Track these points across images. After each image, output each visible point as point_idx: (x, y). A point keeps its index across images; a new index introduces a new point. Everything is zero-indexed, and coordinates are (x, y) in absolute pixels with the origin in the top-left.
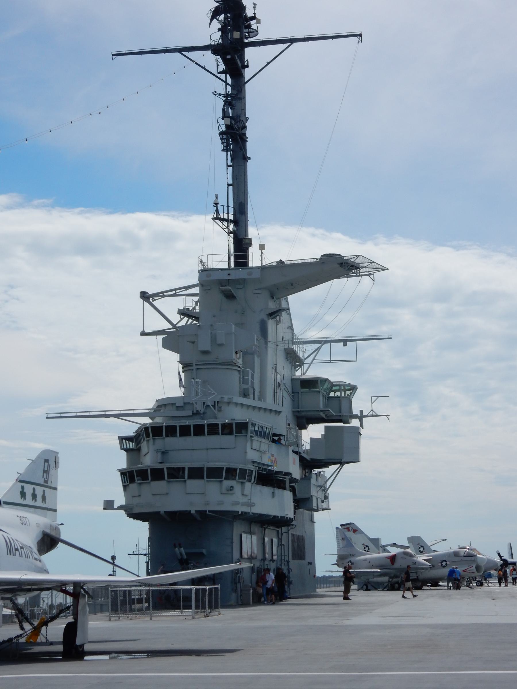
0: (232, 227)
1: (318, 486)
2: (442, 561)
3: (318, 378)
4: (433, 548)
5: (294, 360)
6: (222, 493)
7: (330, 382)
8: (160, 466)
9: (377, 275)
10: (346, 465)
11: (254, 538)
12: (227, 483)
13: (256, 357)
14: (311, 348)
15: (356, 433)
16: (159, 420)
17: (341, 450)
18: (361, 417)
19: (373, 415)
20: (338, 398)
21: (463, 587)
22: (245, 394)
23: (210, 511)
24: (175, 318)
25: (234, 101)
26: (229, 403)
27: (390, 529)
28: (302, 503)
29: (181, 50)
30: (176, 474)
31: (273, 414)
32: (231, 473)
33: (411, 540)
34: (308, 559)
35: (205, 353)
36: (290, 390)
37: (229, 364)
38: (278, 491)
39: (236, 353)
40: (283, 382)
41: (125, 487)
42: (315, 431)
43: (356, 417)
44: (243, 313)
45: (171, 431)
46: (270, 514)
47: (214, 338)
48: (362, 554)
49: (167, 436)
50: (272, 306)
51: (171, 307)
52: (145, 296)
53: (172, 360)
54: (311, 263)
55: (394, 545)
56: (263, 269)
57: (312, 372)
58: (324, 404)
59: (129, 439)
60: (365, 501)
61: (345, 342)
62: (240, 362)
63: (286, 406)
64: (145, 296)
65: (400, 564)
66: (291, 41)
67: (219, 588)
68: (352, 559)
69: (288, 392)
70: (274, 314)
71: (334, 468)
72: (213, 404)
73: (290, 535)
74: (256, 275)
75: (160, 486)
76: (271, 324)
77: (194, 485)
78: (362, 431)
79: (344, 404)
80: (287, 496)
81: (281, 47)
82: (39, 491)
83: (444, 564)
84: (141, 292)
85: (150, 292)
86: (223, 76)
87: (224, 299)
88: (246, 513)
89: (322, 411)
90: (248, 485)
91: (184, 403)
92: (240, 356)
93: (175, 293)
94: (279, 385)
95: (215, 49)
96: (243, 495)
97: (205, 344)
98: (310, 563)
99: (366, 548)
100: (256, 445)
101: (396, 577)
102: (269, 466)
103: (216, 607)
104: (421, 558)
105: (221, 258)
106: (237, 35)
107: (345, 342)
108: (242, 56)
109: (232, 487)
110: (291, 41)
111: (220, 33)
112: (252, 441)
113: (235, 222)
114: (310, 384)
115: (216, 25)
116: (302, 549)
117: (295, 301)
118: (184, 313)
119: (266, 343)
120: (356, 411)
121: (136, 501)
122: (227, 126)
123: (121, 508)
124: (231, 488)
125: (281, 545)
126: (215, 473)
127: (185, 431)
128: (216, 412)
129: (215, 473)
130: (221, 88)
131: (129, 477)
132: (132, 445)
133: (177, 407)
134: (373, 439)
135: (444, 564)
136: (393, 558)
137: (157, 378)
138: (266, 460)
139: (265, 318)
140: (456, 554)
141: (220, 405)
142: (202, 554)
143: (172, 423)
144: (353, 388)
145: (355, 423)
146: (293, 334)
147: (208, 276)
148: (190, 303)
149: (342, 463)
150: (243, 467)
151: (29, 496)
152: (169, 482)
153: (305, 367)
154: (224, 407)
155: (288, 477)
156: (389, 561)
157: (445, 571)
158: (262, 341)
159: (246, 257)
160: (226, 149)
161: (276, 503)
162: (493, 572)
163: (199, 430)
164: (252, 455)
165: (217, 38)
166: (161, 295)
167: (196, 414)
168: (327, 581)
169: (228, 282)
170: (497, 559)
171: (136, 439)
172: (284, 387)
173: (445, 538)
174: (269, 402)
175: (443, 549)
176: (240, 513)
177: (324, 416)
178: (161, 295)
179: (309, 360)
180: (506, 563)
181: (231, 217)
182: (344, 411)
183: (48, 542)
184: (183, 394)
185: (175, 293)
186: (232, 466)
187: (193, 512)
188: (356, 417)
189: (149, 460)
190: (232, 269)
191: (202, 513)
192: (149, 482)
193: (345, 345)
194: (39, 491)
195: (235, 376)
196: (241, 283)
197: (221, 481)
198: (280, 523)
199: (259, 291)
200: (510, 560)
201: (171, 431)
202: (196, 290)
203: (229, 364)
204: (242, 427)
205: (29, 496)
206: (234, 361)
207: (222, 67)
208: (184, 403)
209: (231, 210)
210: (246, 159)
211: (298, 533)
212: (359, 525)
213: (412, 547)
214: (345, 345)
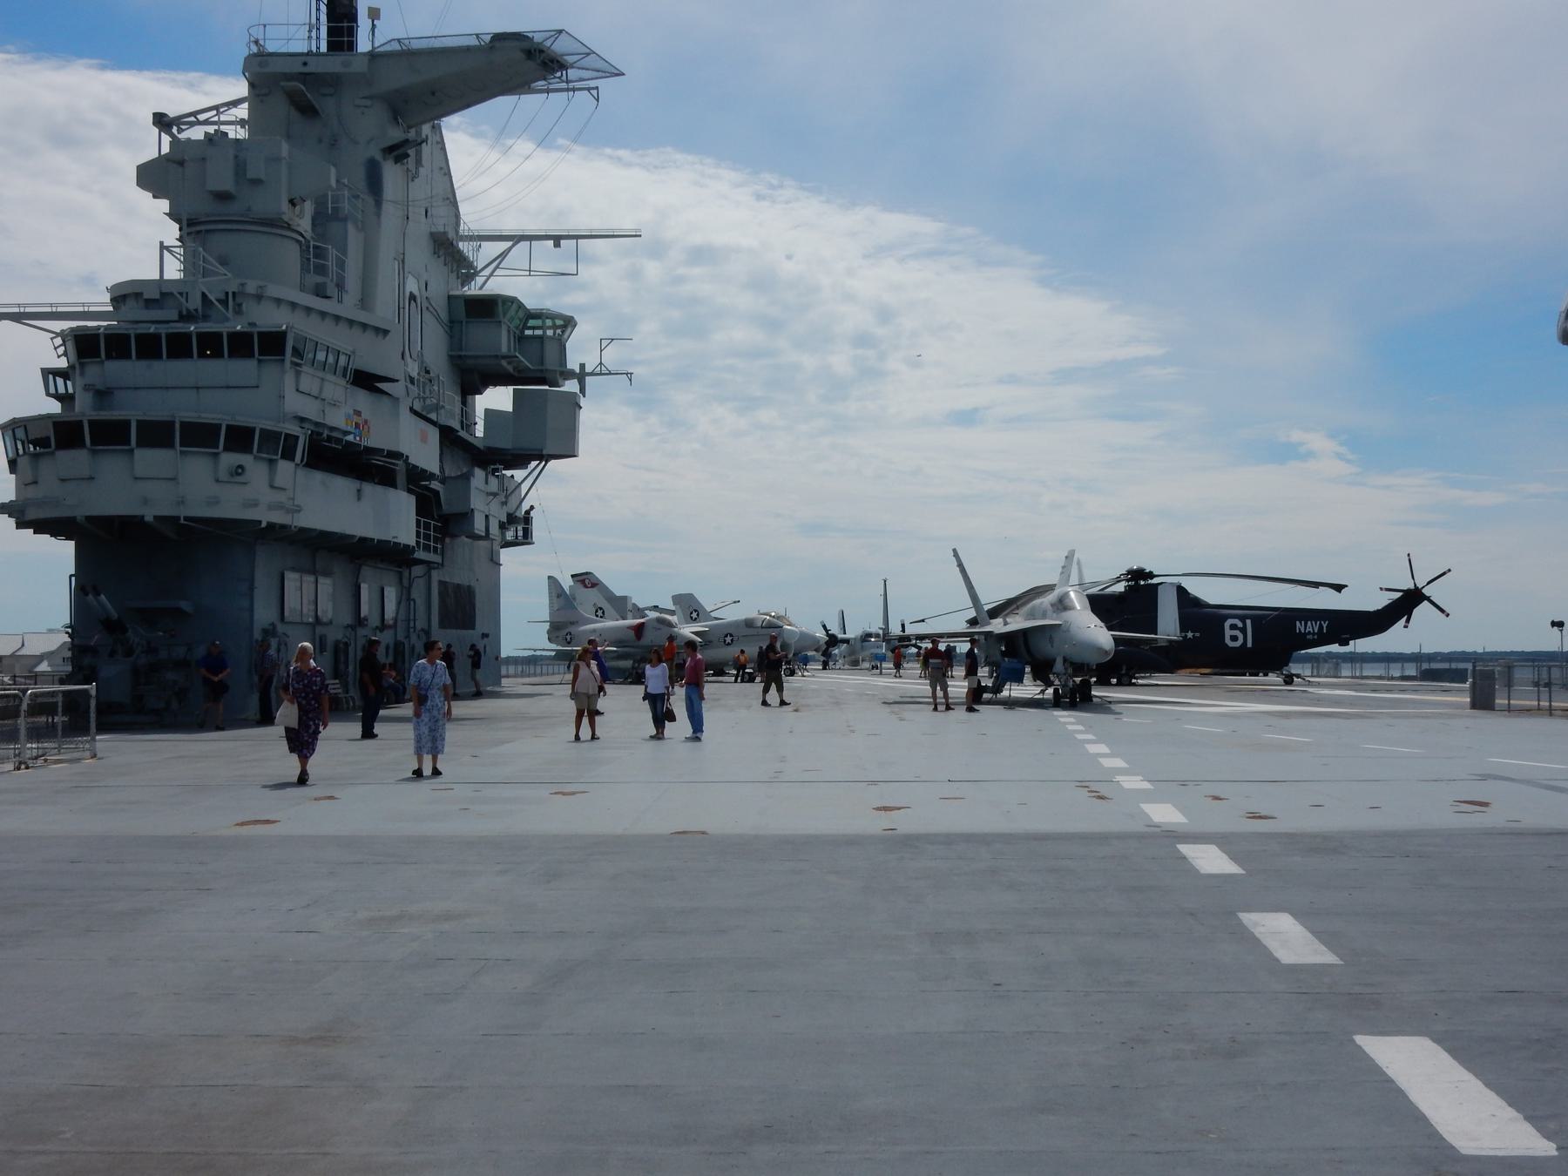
1: (489, 494)
2: (729, 634)
3: (499, 296)
5: (463, 268)
6: (217, 481)
7: (521, 306)
10: (552, 463)
11: (325, 585)
12: (229, 459)
13: (351, 228)
14: (492, 249)
17: (543, 436)
18: (581, 376)
20: (541, 338)
23: (186, 519)
26: (259, 297)
27: (646, 581)
28: (443, 520)
31: (370, 334)
32: (240, 438)
33: (677, 599)
34: (481, 626)
35: (223, 197)
36: (444, 315)
37: (275, 224)
38: (368, 488)
39: (292, 202)
40: (425, 294)
42: (498, 398)
43: (570, 375)
44: (334, 143)
46: (348, 532)
49: (109, 357)
50: (395, 134)
54: (468, 49)
55: (656, 608)
57: (498, 285)
58: (513, 357)
61: (558, 240)
62: (305, 225)
63: (433, 345)
67: (93, 693)
68: (572, 629)
69: (438, 318)
72: (222, 297)
74: (359, 66)
76: (391, 174)
77: (150, 460)
78: (583, 402)
83: (728, 639)
84: (155, 115)
87: (295, 114)
88: (283, 527)
89: (504, 357)
90: (284, 467)
91: (162, 294)
92: (302, 211)
94: (413, 297)
96: (272, 487)
98: (485, 636)
99: (600, 612)
102: (347, 433)
109: (240, 467)
112: (298, 374)
114: (487, 308)
116: (467, 608)
119: (378, 203)
120: (573, 364)
121: (32, 493)
124: (239, 470)
125: (409, 599)
126: (200, 436)
128: (230, 314)
129: (200, 436)
133: (148, 301)
134: (599, 420)
135: (728, 639)
136: (639, 630)
138: (337, 419)
139: (379, 157)
140: (749, 623)
141: (238, 300)
142: (179, 611)
145: (571, 386)
146: (457, 216)
147: (261, 65)
149: (545, 458)
150: (269, 425)
152: (94, 452)
155: (400, 463)
156: (632, 633)
157: (752, 651)
158: (370, 200)
162: (810, 653)
164: (296, 404)
168: (530, 663)
169: (304, 77)
170: (821, 634)
172: (425, 304)
175: (732, 615)
176: (264, 525)
177: (510, 369)
179: (487, 272)
180: (833, 641)
182: (551, 363)
186: (242, 420)
187: (149, 518)
190: (318, 54)
192: (52, 453)
193: (557, 245)
195: (290, 255)
196: (330, 83)
197: (216, 455)
199: (368, 102)
200: (841, 636)
203: (275, 224)
204: (272, 344)
206: (285, 218)
208: (162, 294)
211: (457, 580)
213: (679, 612)
214: (557, 245)
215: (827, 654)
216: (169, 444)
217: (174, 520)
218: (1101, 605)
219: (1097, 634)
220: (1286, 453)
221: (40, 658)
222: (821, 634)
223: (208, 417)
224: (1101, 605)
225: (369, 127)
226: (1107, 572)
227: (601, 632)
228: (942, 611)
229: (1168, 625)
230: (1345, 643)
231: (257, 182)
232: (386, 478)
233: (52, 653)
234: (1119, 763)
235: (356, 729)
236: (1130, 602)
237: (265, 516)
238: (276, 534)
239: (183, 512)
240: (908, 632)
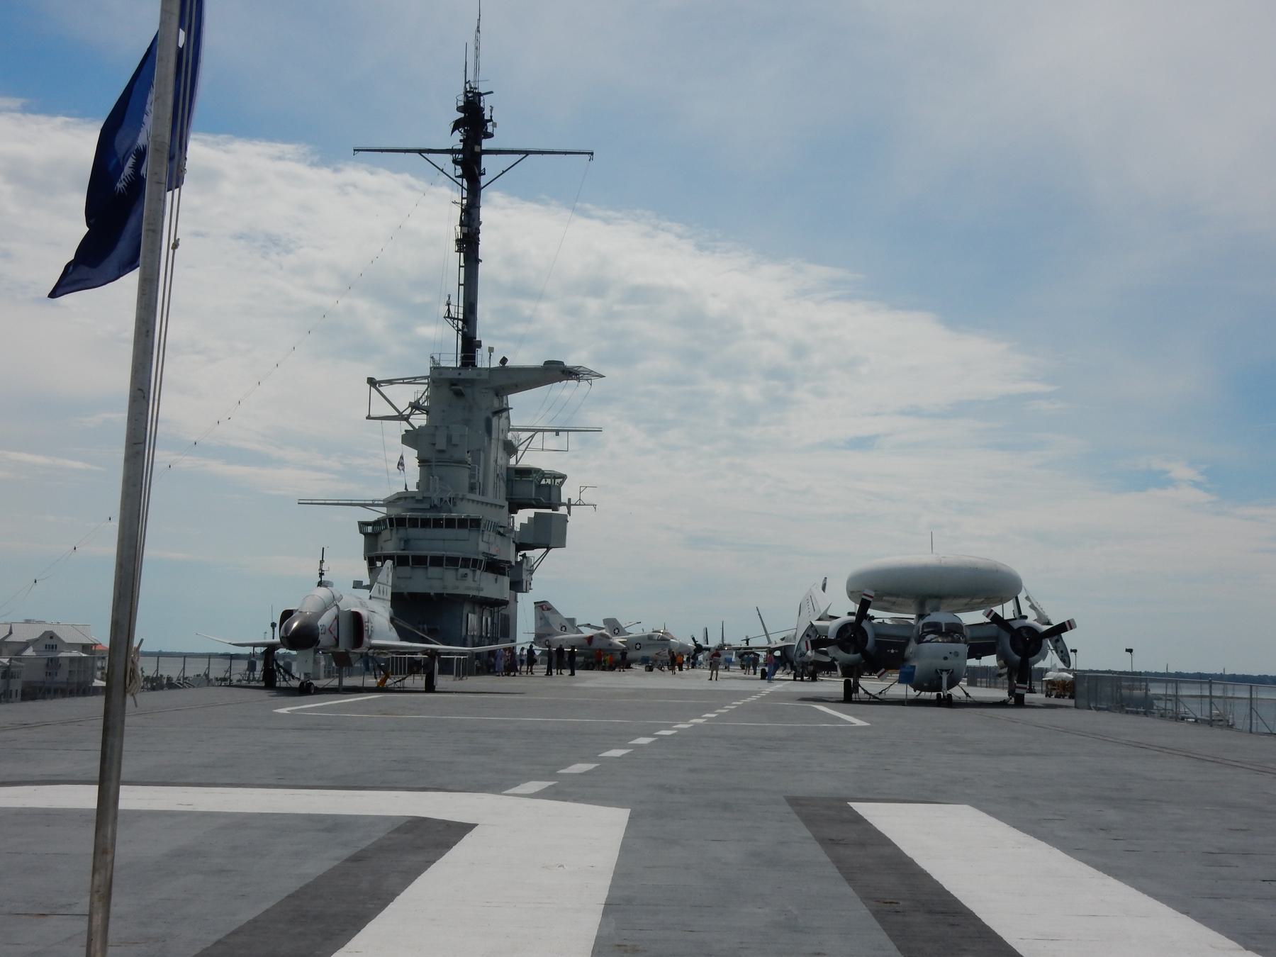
2: (638, 644)
4: (627, 630)
5: (510, 449)
8: (406, 553)
12: (462, 571)
15: (564, 519)
17: (548, 534)
19: (580, 504)
21: (655, 669)
29: (420, 152)
33: (606, 621)
35: (442, 451)
37: (461, 462)
42: (523, 516)
43: (564, 504)
45: (414, 523)
47: (449, 439)
48: (559, 634)
52: (372, 382)
53: (411, 456)
57: (527, 459)
58: (537, 490)
60: (571, 584)
64: (372, 382)
65: (595, 645)
66: (527, 153)
71: (539, 552)
73: (499, 615)
74: (485, 376)
76: (495, 421)
77: (434, 571)
79: (554, 493)
80: (506, 581)
81: (519, 157)
85: (378, 379)
86: (459, 180)
90: (478, 572)
97: (441, 444)
99: (564, 628)
100: (486, 538)
101: (591, 657)
103: (464, 674)
104: (617, 640)
105: (451, 360)
107: (557, 432)
108: (479, 163)
110: (527, 153)
114: (525, 473)
116: (505, 628)
117: (514, 399)
119: (490, 439)
120: (564, 499)
122: (464, 235)
126: (453, 562)
127: (425, 523)
129: (453, 562)
132: (370, 529)
134: (577, 523)
136: (590, 639)
137: (395, 471)
138: (493, 551)
140: (650, 637)
143: (415, 515)
144: (564, 477)
145: (563, 510)
153: (520, 453)
154: (458, 503)
159: (474, 358)
161: (492, 587)
163: (437, 523)
164: (483, 547)
166: (390, 382)
167: (433, 508)
173: (639, 620)
174: (489, 498)
175: (636, 632)
178: (390, 382)
180: (699, 649)
181: (461, 317)
182: (554, 500)
184: (418, 487)
186: (468, 556)
188: (564, 504)
191: (439, 596)
195: (466, 473)
196: (471, 382)
200: (704, 646)
201: (414, 523)
203: (461, 462)
204: (475, 524)
209: (461, 310)
210: (477, 261)
215: (695, 658)
216: (441, 565)
217: (441, 595)
220: (1159, 480)
221: (26, 645)
222: (691, 644)
227: (567, 640)
228: (784, 625)
230: (979, 658)
231: (456, 445)
233: (36, 640)
235: (569, 672)
237: (472, 593)
238: (463, 599)
239: (446, 592)
240: (751, 645)
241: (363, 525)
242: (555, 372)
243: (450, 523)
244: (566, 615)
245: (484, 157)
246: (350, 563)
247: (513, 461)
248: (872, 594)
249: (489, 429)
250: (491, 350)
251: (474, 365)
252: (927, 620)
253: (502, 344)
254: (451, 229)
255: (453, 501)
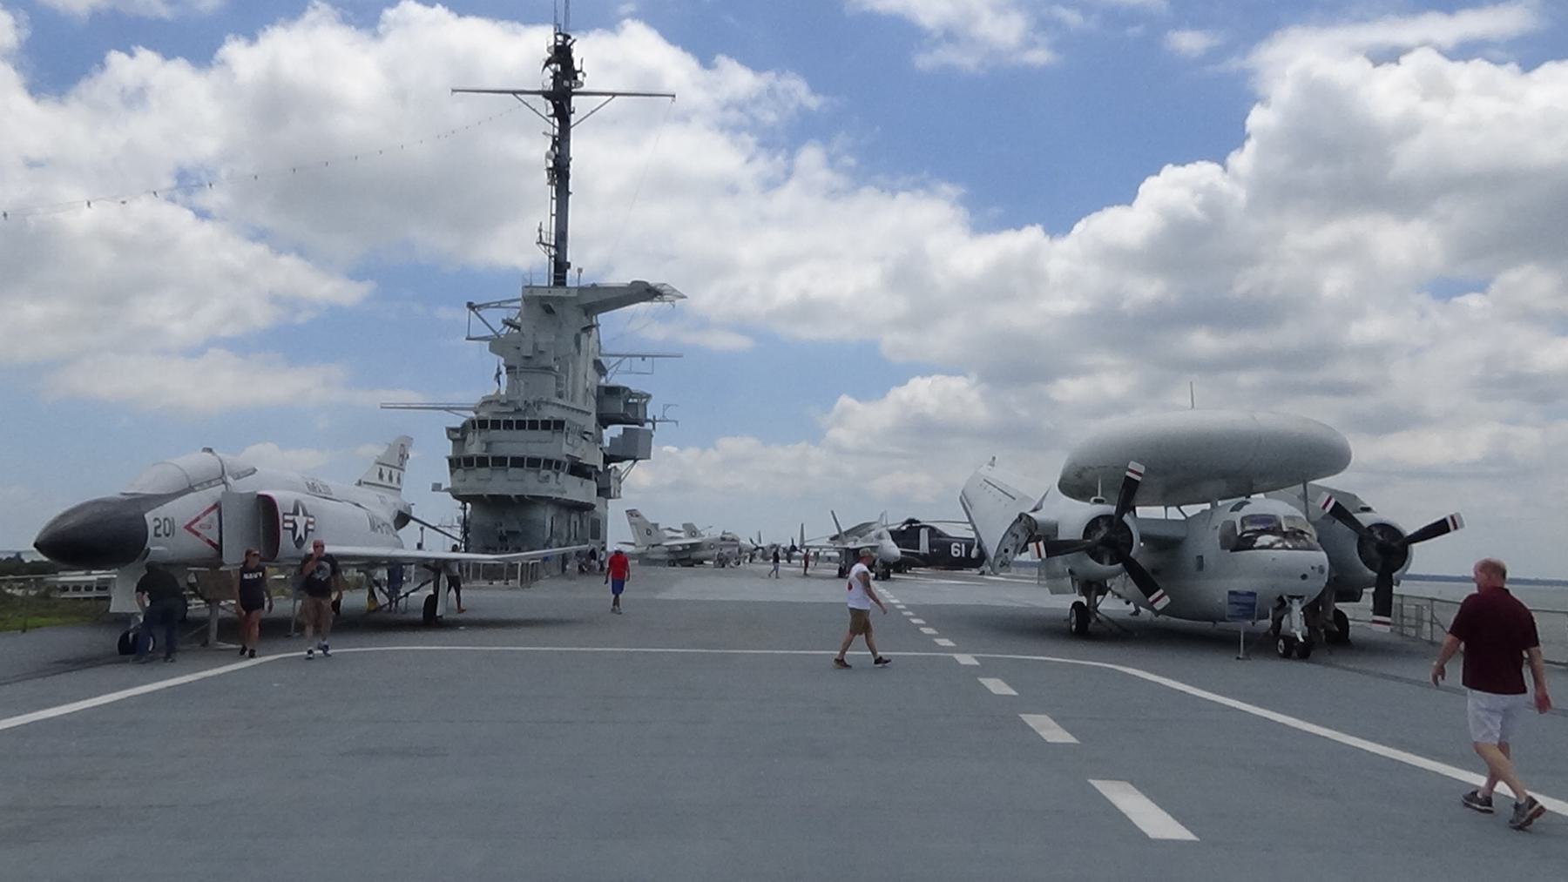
0: (553, 252)
5: (600, 368)
9: (678, 302)
12: (544, 472)
14: (614, 360)
16: (484, 415)
17: (632, 449)
22: (560, 396)
24: (498, 326)
25: (561, 142)
28: (604, 492)
29: (514, 93)
30: (500, 462)
37: (548, 369)
41: (452, 472)
42: (614, 431)
44: (560, 326)
45: (496, 425)
47: (535, 346)
51: (496, 318)
52: (471, 306)
56: (581, 289)
57: (614, 380)
58: (620, 406)
59: (455, 430)
60: (659, 490)
63: (591, 406)
64: (471, 306)
66: (614, 95)
70: (587, 329)
74: (574, 294)
75: (484, 472)
76: (584, 336)
82: (395, 473)
93: (499, 305)
95: (546, 95)
97: (527, 350)
105: (544, 279)
106: (566, 83)
110: (614, 95)
111: (721, 60)
113: (556, 247)
114: (613, 391)
115: (549, 72)
117: (602, 318)
118: (507, 323)
120: (649, 417)
123: (447, 490)
126: (534, 463)
127: (508, 425)
130: (550, 129)
131: (454, 463)
134: (663, 448)
137: (479, 380)
143: (497, 418)
144: (649, 397)
145: (648, 426)
148: (513, 315)
151: (386, 477)
160: (551, 183)
163: (521, 425)
164: (566, 450)
165: (549, 85)
166: (487, 306)
167: (518, 411)
171: (464, 429)
178: (487, 306)
180: (794, 548)
182: (640, 415)
183: (403, 519)
185: (499, 305)
189: (474, 448)
194: (395, 473)
196: (561, 300)
198: (583, 508)
201: (496, 425)
202: (519, 304)
204: (559, 424)
205: (386, 477)
207: (552, 111)
210: (568, 193)
212: (641, 511)
218: (896, 536)
219: (893, 550)
223: (538, 455)
224: (896, 536)
225: (575, 320)
226: (897, 521)
229: (924, 547)
232: (588, 477)
234: (915, 621)
236: (907, 534)
237: (554, 495)
241: (451, 431)
242: (646, 292)
243: (533, 425)
244: (651, 521)
245: (574, 98)
246: (431, 462)
247: (603, 381)
248: (1142, 469)
249: (578, 344)
250: (580, 270)
251: (564, 284)
252: (1247, 510)
253: (592, 262)
254: (539, 150)
255: (539, 404)
